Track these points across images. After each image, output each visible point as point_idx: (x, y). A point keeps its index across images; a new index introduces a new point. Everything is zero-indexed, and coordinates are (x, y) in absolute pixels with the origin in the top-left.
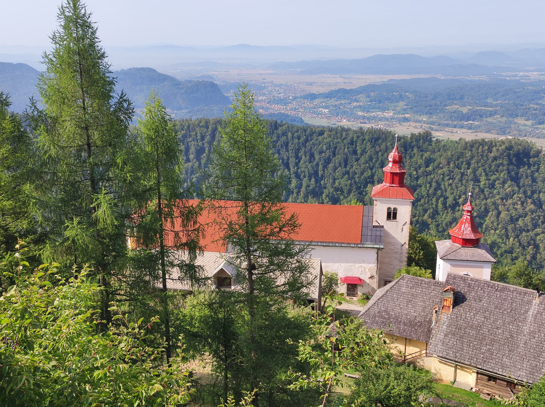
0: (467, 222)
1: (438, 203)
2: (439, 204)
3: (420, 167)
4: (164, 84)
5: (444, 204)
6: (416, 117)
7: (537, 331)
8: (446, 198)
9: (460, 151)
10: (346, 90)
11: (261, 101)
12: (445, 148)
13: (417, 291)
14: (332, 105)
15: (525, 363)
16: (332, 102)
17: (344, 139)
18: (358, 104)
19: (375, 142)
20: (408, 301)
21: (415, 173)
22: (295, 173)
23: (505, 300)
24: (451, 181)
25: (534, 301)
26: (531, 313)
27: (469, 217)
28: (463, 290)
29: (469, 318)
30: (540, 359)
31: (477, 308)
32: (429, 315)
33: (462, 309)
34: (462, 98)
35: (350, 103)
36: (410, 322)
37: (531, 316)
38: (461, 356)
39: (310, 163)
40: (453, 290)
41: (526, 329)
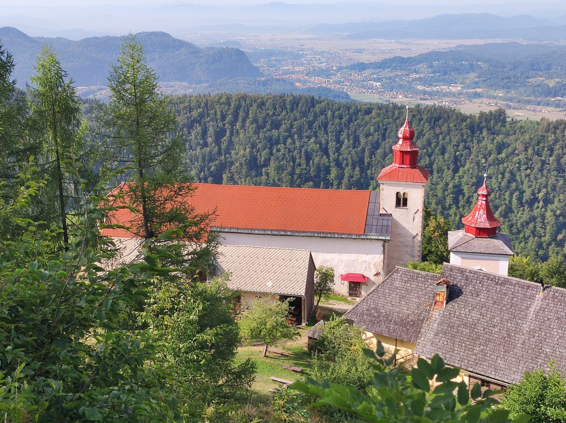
0: (482, 208)
1: (512, 198)
2: (514, 199)
3: (490, 154)
4: (180, 52)
5: (520, 199)
6: (490, 92)
7: (538, 329)
8: (522, 192)
9: (541, 133)
10: (403, 59)
11: (298, 72)
12: (523, 130)
13: (412, 285)
14: (385, 77)
15: (521, 365)
16: (386, 73)
17: (396, 119)
18: (417, 76)
19: (434, 123)
20: (401, 297)
21: (483, 161)
22: (335, 161)
23: (505, 294)
24: (528, 171)
25: (537, 296)
26: (533, 310)
27: (484, 202)
28: (460, 283)
29: (463, 315)
30: (539, 360)
31: (473, 303)
32: (424, 313)
33: (456, 305)
34: (548, 68)
35: (408, 75)
36: (402, 320)
37: (532, 312)
38: (450, 358)
39: (353, 148)
40: (447, 283)
41: (526, 327)
